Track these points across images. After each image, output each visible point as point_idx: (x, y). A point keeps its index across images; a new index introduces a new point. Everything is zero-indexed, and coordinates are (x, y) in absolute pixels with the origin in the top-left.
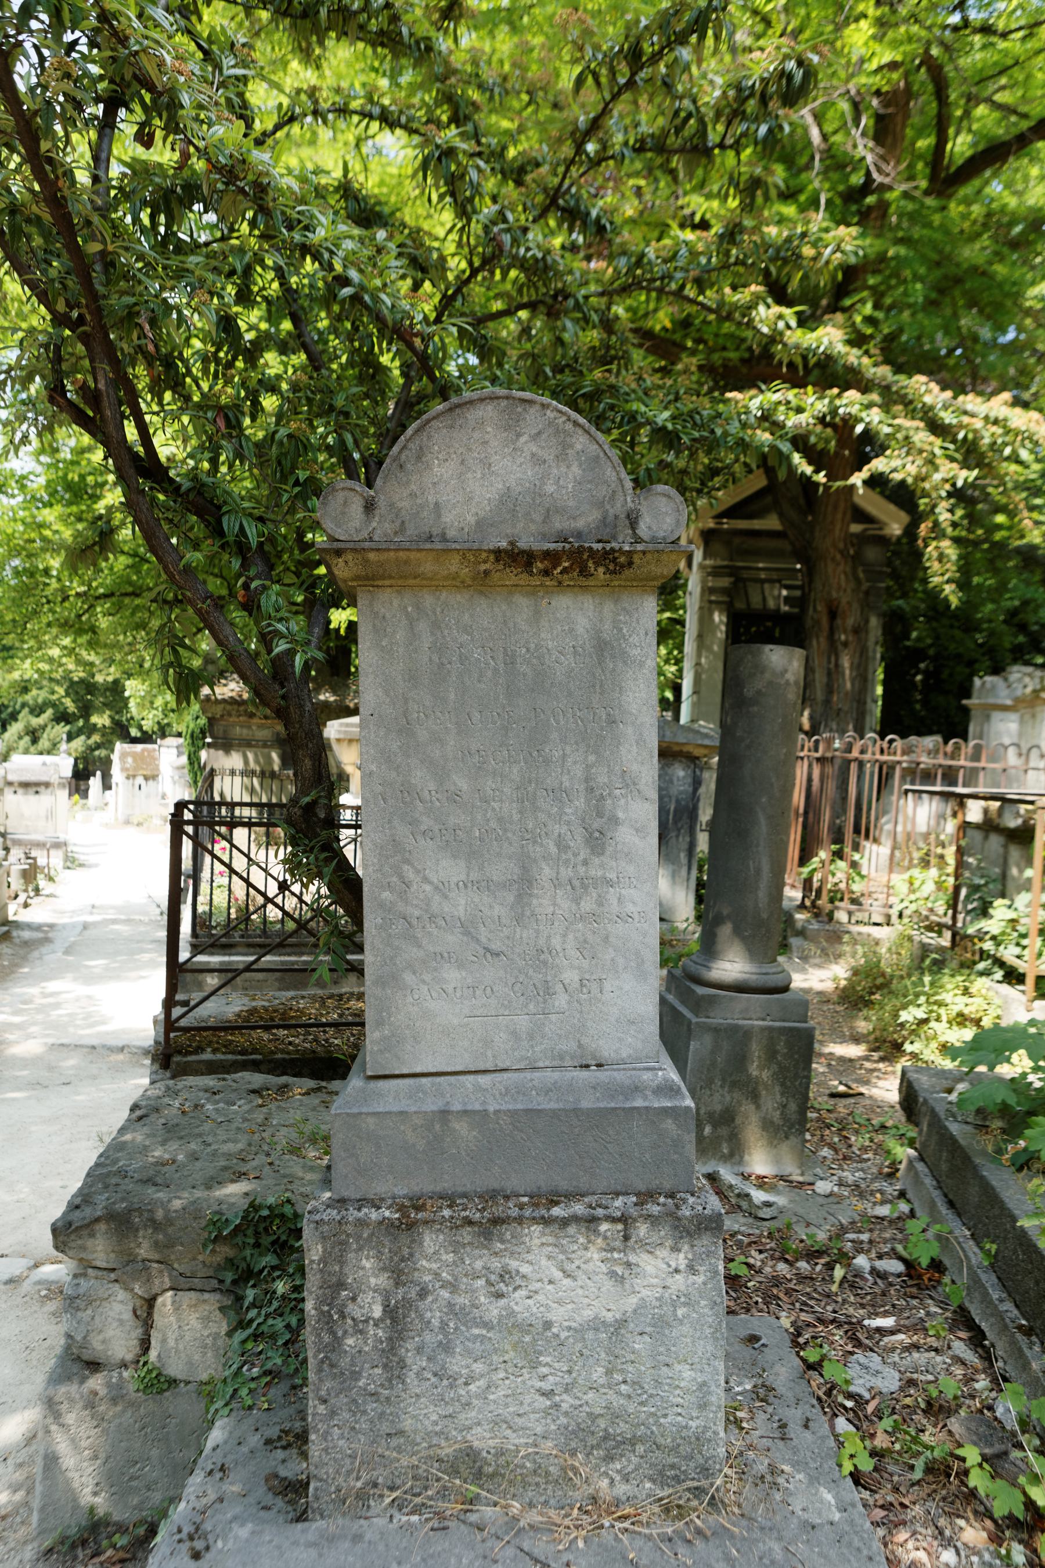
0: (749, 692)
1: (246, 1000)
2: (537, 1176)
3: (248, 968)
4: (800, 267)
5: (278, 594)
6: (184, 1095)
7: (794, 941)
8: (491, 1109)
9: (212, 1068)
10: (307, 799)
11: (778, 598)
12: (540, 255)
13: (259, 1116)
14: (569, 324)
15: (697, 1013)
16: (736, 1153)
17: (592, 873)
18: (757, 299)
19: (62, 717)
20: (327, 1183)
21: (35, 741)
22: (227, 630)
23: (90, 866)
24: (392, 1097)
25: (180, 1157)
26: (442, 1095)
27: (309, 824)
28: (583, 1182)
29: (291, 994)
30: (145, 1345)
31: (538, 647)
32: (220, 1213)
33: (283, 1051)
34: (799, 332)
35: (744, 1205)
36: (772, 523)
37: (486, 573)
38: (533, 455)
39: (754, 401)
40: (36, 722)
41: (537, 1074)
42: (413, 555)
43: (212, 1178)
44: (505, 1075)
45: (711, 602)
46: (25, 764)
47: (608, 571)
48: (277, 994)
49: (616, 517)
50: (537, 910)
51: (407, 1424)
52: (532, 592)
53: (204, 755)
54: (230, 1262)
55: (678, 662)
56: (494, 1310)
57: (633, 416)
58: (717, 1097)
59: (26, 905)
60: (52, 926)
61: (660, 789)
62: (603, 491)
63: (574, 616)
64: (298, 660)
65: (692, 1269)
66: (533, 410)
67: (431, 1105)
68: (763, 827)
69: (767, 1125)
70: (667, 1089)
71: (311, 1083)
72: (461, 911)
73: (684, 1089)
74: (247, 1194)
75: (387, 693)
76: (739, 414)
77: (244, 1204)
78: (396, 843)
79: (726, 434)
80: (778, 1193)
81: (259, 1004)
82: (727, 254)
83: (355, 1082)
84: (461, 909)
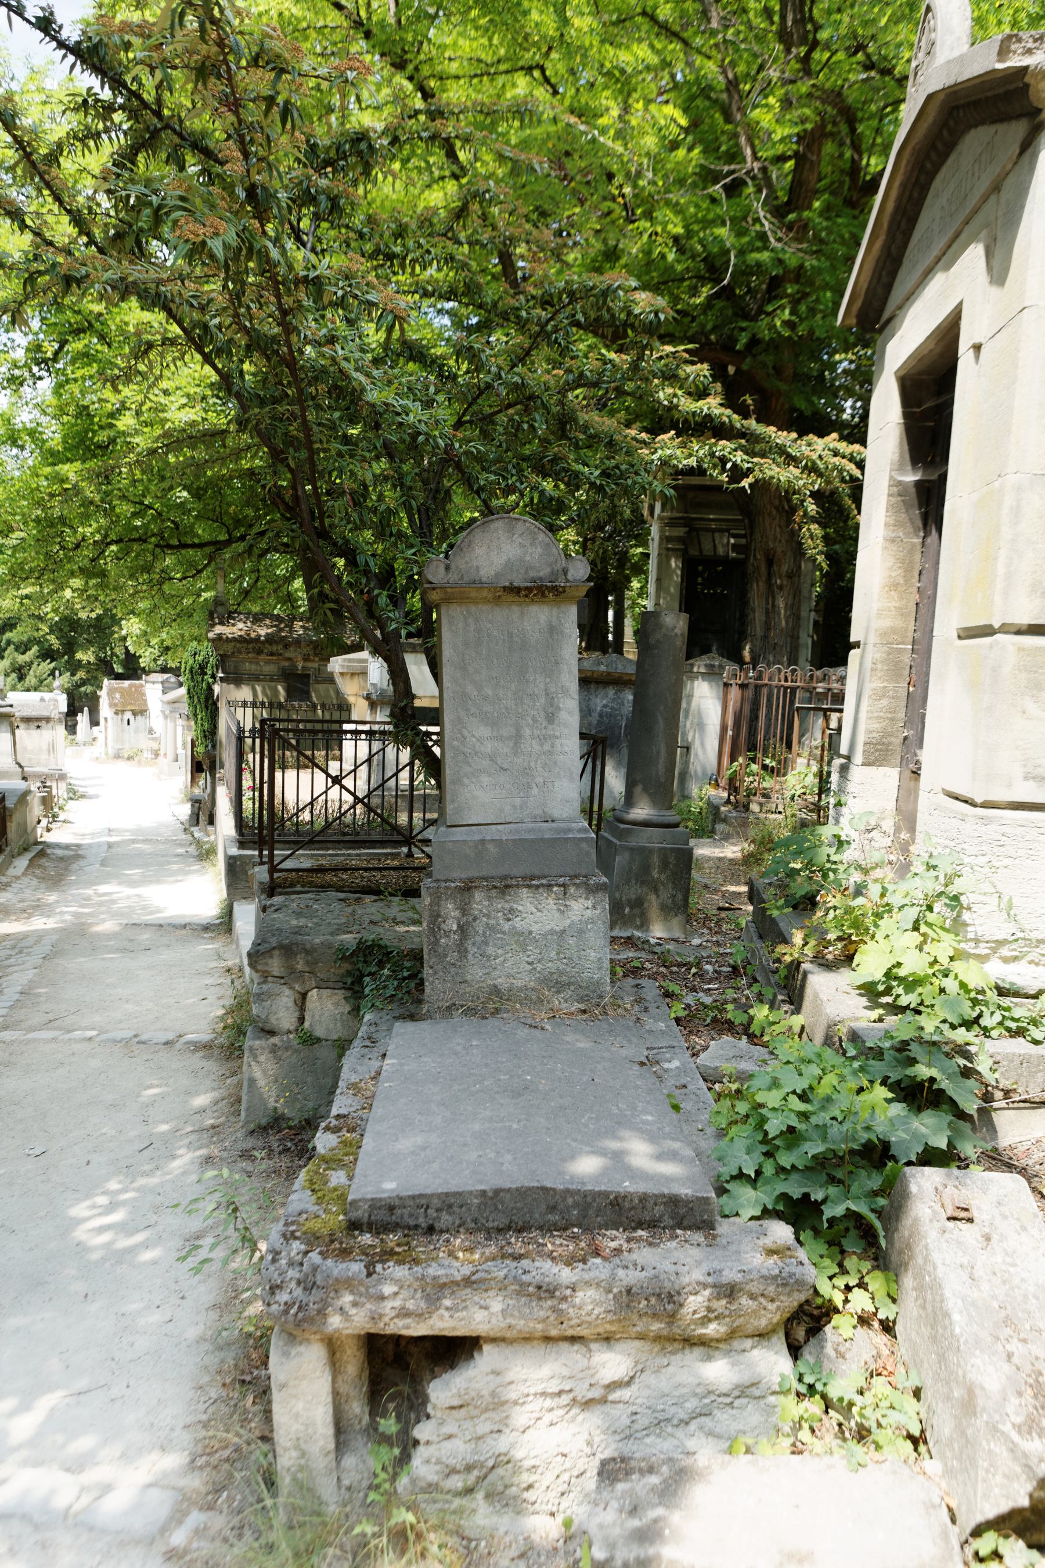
0: (652, 641)
2: (524, 866)
16: (644, 925)
19: (48, 654)
21: (21, 678)
23: (90, 797)
28: (546, 872)
30: (301, 1020)
40: (21, 659)
46: (22, 701)
51: (469, 977)
52: (520, 604)
54: (349, 973)
56: (506, 926)
59: (48, 830)
60: (78, 846)
65: (594, 907)
67: (477, 838)
68: (661, 724)
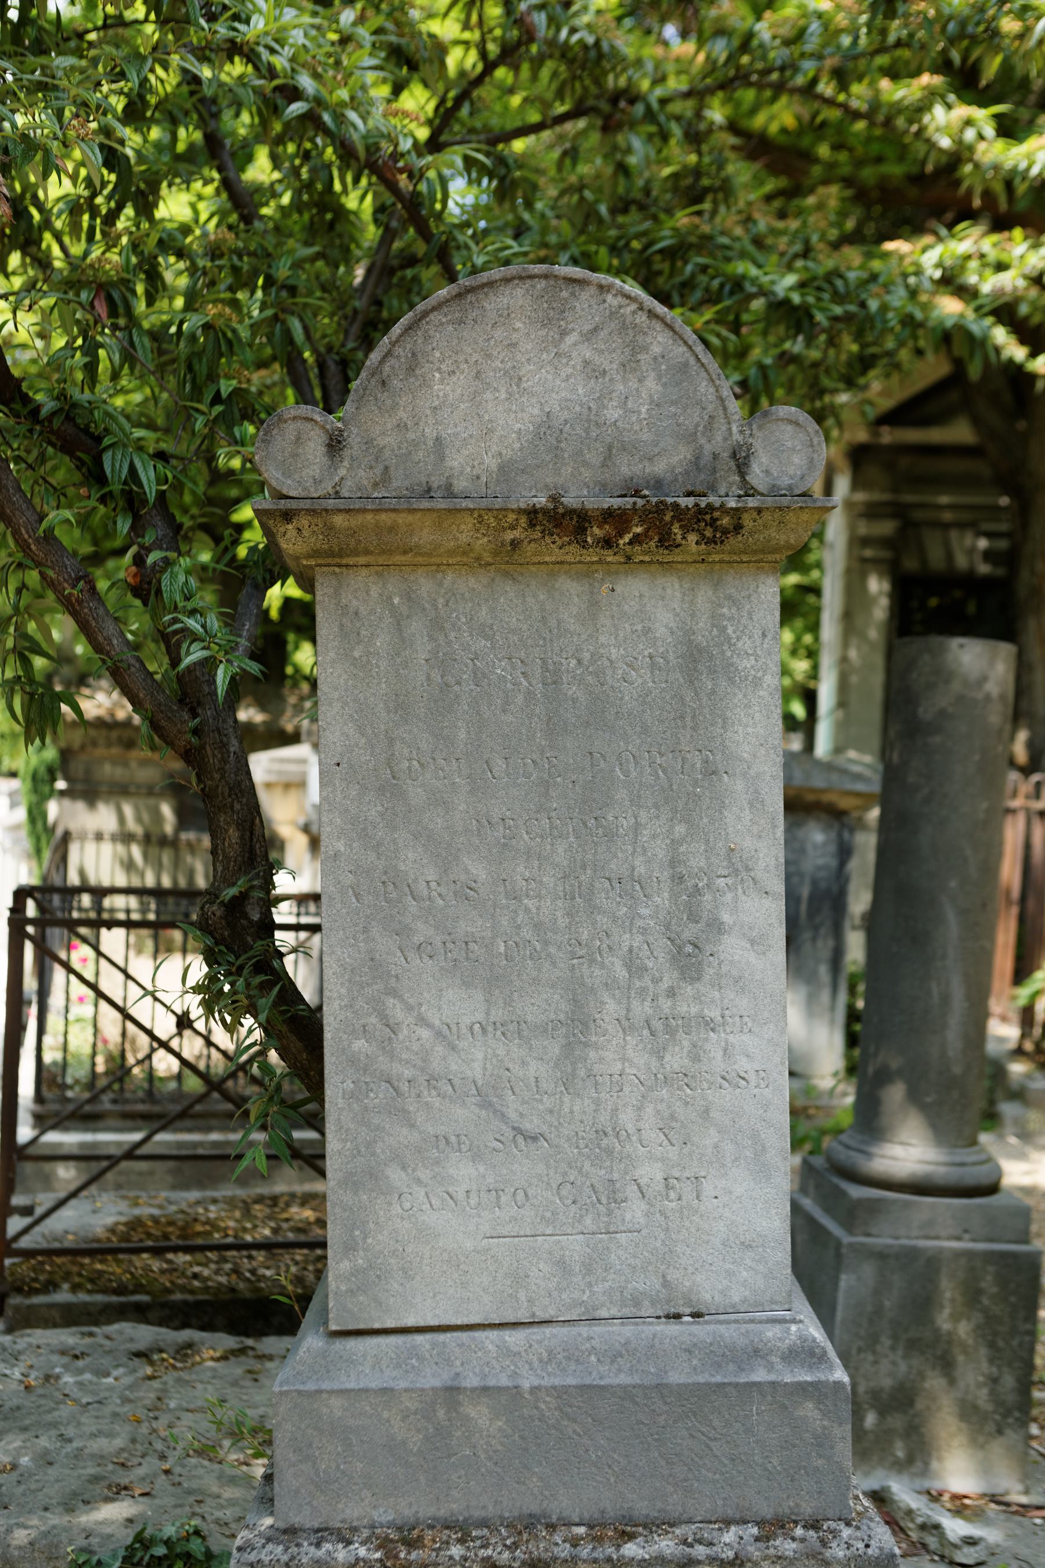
0: (926, 712)
1: (123, 1206)
3: (131, 1153)
4: (998, 49)
5: (188, 572)
6: (28, 1359)
7: (1008, 1109)
8: (526, 1385)
9: (70, 1317)
10: (233, 891)
11: (971, 551)
12: (590, 40)
13: (148, 1394)
14: (637, 143)
15: (850, 1229)
16: (918, 1455)
17: (683, 1009)
18: (932, 96)
20: (267, 1503)
22: (110, 628)
24: (369, 1364)
25: (25, 1460)
26: (449, 1363)
27: (229, 924)
28: (674, 1503)
29: (194, 1195)
31: (595, 657)
32: (88, 1551)
33: (183, 1289)
34: (1000, 145)
35: (932, 1542)
36: (960, 432)
37: (515, 544)
38: (586, 363)
39: (928, 255)
41: (598, 1329)
42: (402, 519)
43: (75, 1494)
44: (548, 1330)
45: (864, 560)
47: (703, 540)
48: (175, 1195)
49: (715, 456)
50: (597, 1068)
52: (586, 572)
53: (53, 809)
55: (812, 654)
57: (738, 284)
58: (885, 1365)
61: (787, 863)
62: (694, 418)
63: (651, 608)
64: (222, 677)
66: (586, 295)
67: (432, 1379)
68: (952, 926)
69: (968, 1412)
70: (805, 1354)
71: (228, 1341)
72: (476, 1071)
73: (832, 1353)
74: (130, 1521)
75: (361, 730)
76: (905, 276)
77: (127, 1536)
78: (375, 964)
79: (884, 308)
80: (987, 1522)
81: (145, 1211)
82: (884, 32)
83: (310, 1342)
84: (477, 1066)
